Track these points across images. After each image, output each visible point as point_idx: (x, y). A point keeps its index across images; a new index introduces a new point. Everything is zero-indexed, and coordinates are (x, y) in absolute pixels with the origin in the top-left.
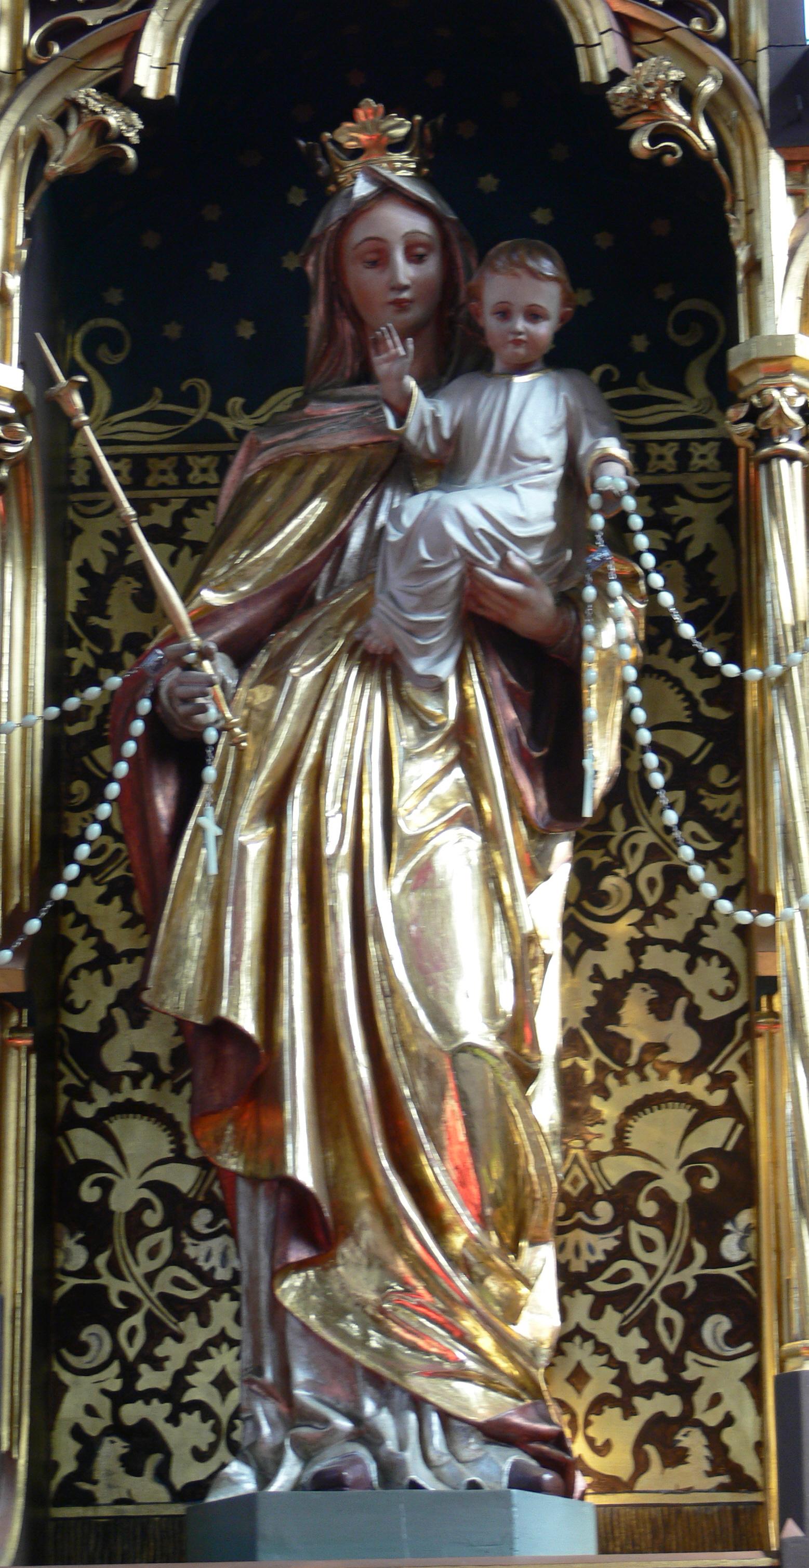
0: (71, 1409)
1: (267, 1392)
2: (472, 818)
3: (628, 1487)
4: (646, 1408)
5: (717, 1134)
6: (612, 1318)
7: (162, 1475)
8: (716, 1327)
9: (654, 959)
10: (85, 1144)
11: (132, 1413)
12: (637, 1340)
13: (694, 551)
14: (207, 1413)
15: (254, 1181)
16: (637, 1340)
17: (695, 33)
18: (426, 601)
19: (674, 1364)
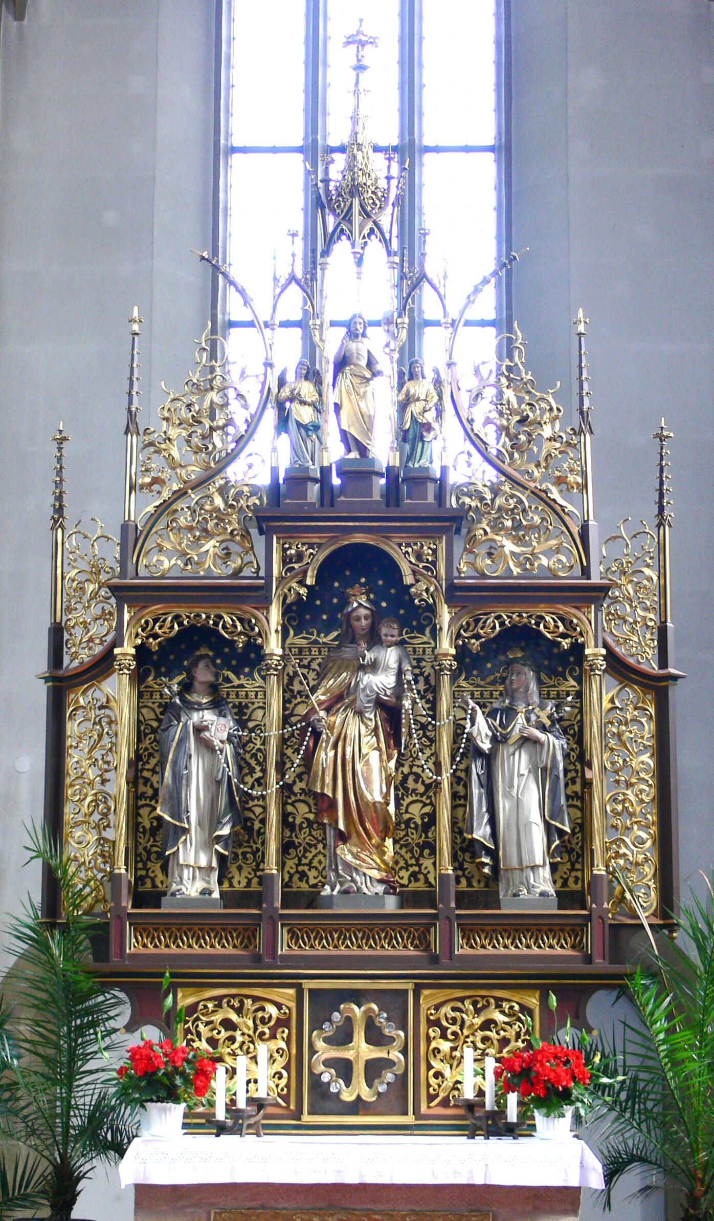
0: (287, 868)
1: (333, 870)
2: (378, 749)
3: (407, 886)
4: (411, 869)
5: (427, 809)
6: (404, 850)
7: (307, 882)
8: (427, 852)
9: (415, 769)
10: (290, 808)
11: (300, 868)
12: (409, 855)
13: (426, 674)
14: (316, 869)
15: (330, 825)
16: (409, 855)
17: (428, 1034)
18: (368, 702)
19: (417, 860)
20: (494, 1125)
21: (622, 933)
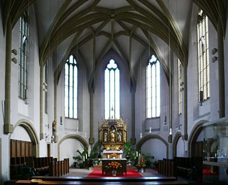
20: (118, 150)
21: (124, 143)
